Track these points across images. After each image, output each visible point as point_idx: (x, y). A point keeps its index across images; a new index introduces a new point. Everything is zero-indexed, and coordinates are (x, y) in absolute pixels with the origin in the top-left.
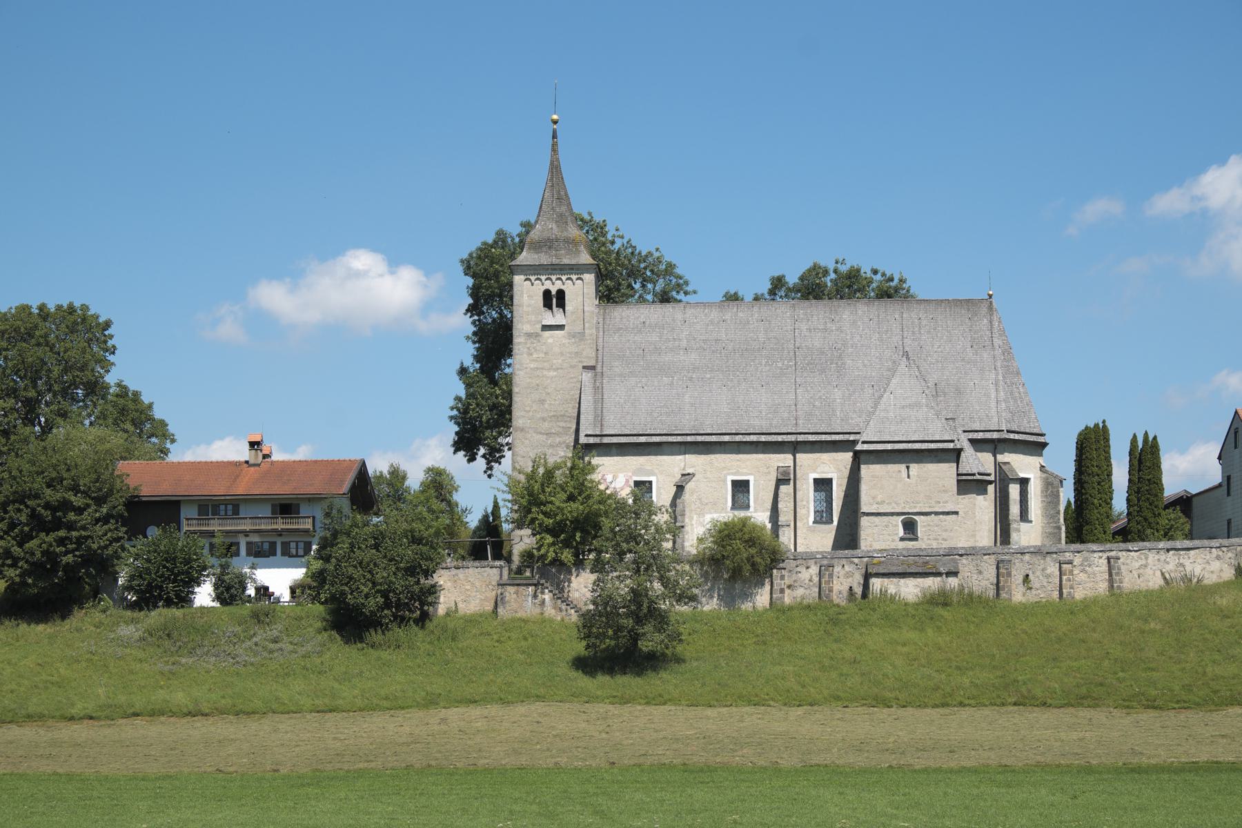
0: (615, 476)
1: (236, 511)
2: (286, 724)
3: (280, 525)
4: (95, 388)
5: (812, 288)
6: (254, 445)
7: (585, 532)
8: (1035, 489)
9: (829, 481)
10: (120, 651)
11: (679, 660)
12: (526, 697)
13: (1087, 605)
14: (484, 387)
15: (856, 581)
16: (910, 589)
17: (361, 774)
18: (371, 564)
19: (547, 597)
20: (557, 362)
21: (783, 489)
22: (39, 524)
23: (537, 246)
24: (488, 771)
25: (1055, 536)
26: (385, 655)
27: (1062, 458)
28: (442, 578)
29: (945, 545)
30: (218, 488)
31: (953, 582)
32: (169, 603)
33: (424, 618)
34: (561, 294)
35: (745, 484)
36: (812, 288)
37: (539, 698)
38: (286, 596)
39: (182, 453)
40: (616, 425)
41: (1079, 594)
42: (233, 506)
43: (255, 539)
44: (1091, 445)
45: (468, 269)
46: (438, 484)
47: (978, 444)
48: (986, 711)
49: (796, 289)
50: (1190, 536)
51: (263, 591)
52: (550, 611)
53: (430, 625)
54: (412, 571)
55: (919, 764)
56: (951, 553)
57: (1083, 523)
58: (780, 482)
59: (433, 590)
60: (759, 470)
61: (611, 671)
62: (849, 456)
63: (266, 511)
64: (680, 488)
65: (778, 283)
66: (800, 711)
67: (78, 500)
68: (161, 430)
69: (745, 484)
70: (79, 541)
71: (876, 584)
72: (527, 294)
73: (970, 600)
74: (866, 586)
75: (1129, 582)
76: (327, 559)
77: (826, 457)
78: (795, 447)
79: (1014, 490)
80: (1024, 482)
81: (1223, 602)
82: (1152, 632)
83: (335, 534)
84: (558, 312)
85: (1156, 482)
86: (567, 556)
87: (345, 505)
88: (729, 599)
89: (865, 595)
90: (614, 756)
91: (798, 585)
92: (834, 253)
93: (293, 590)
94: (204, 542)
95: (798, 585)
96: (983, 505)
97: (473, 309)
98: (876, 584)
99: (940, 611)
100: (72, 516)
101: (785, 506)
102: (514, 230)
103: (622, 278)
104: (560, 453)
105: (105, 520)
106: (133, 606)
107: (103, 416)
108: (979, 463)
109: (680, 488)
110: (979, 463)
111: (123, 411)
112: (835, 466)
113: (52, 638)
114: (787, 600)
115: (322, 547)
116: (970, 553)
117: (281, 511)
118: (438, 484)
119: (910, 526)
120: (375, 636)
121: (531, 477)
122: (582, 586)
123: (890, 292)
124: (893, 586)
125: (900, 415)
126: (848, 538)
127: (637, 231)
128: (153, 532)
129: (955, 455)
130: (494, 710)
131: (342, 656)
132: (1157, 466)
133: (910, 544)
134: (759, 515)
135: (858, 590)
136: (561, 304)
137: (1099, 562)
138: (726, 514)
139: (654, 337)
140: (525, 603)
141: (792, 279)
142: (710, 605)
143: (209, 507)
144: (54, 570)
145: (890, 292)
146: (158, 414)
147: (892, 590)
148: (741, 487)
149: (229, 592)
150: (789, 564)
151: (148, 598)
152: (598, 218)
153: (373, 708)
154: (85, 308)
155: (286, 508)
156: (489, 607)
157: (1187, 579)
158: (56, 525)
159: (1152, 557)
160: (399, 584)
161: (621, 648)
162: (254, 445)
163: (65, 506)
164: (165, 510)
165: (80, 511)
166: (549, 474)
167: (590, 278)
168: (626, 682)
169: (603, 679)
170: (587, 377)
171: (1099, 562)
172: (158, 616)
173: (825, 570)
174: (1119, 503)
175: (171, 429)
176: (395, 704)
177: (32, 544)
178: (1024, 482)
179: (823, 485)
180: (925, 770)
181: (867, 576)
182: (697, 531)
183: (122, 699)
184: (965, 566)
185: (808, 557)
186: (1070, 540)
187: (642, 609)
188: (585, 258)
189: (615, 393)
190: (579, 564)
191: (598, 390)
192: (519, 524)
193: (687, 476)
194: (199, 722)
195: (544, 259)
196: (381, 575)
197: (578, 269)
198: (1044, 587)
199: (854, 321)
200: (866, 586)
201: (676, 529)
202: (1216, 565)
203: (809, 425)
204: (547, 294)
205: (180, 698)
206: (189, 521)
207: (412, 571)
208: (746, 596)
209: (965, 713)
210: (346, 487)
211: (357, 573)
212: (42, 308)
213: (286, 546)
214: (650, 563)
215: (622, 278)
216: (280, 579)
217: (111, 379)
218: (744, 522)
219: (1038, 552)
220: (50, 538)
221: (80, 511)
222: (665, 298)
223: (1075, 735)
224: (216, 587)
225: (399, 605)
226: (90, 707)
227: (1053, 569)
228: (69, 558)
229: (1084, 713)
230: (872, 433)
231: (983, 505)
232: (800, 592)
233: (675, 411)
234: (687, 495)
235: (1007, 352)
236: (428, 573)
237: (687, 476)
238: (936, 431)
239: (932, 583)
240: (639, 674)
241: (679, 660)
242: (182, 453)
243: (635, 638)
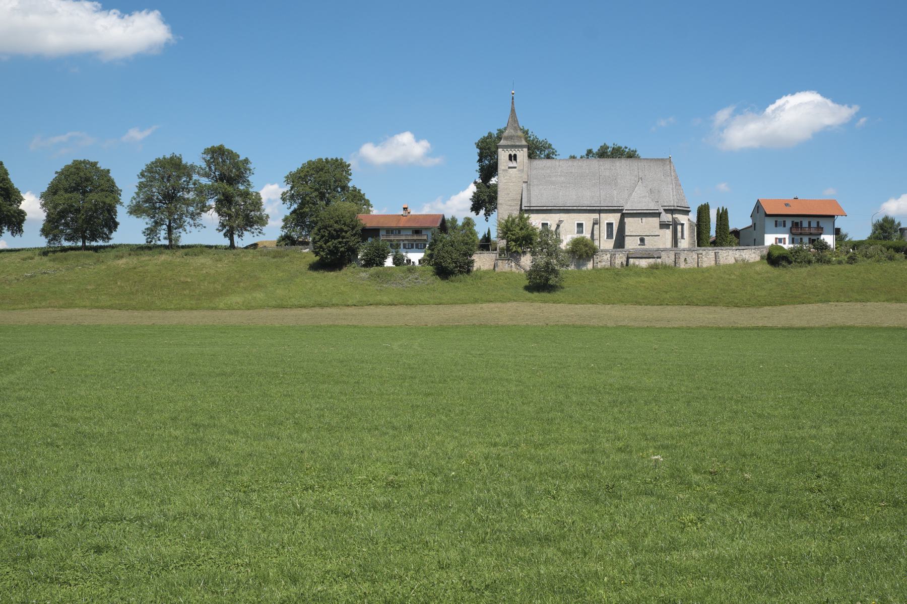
0: (536, 221)
1: (399, 232)
2: (425, 309)
3: (415, 237)
4: (344, 188)
5: (603, 154)
7: (526, 241)
8: (686, 227)
9: (612, 224)
10: (361, 282)
11: (563, 288)
12: (510, 300)
13: (708, 269)
14: (484, 189)
15: (624, 260)
16: (644, 263)
17: (457, 327)
18: (450, 253)
19: (513, 264)
20: (514, 180)
21: (596, 226)
22: (332, 237)
23: (507, 138)
24: (502, 326)
25: (694, 244)
26: (456, 284)
27: (693, 216)
28: (475, 257)
29: (655, 247)
30: (393, 224)
31: (659, 260)
32: (377, 265)
33: (469, 271)
34: (515, 156)
35: (582, 224)
36: (603, 154)
37: (515, 301)
38: (417, 263)
39: (374, 211)
40: (535, 203)
41: (705, 265)
42: (398, 231)
43: (406, 242)
44: (703, 211)
45: (478, 146)
46: (468, 223)
47: (666, 211)
48: (677, 307)
49: (597, 154)
50: (739, 244)
51: (409, 261)
52: (514, 269)
53: (472, 274)
54: (465, 255)
55: (658, 326)
56: (658, 250)
57: (701, 239)
58: (594, 224)
59: (472, 262)
60: (587, 220)
61: (538, 291)
62: (619, 215)
63: (410, 233)
64: (558, 226)
65: (589, 152)
66: (609, 306)
67: (346, 228)
68: (367, 203)
69: (582, 224)
70: (346, 243)
71: (631, 261)
72: (503, 155)
73: (665, 267)
74: (627, 261)
75: (722, 261)
76: (433, 250)
77: (611, 215)
78: (600, 211)
79: (679, 228)
80: (682, 225)
81: (758, 268)
82: (733, 279)
83: (435, 241)
84: (514, 162)
85: (727, 225)
86: (519, 250)
87: (437, 230)
88: (578, 266)
89: (627, 265)
90: (547, 322)
91: (603, 261)
93: (420, 261)
94: (388, 243)
95: (603, 261)
96: (668, 233)
97: (480, 161)
98: (631, 261)
99: (655, 271)
100: (344, 234)
101: (596, 232)
102: (495, 133)
103: (537, 150)
104: (516, 213)
105: (354, 235)
106: (364, 266)
107: (348, 198)
108: (667, 217)
109: (558, 226)
110: (667, 217)
111: (355, 196)
112: (614, 219)
113: (336, 277)
114: (599, 266)
115: (430, 246)
116: (665, 250)
117: (417, 232)
118: (468, 223)
119: (642, 240)
120: (453, 278)
121: (507, 221)
122: (526, 261)
123: (631, 155)
124: (637, 262)
125: (638, 200)
126: (620, 243)
127: (540, 134)
128: (370, 240)
129: (658, 215)
130: (499, 304)
131: (440, 284)
132: (727, 219)
133: (642, 247)
134: (587, 235)
135: (625, 263)
136: (515, 158)
137: (712, 254)
138: (576, 236)
139: (548, 171)
140: (505, 266)
141: (595, 150)
142: (572, 268)
143: (390, 231)
144: (337, 253)
145: (631, 155)
146: (366, 197)
147: (637, 263)
148: (580, 225)
149: (398, 261)
150: (600, 253)
151: (369, 263)
152: (526, 129)
153: (456, 303)
154: (341, 159)
155: (417, 231)
156: (492, 268)
157: (743, 260)
158: (338, 237)
159: (731, 252)
160: (461, 259)
161: (541, 283)
162: (543, 224)
163: (342, 230)
164: (374, 232)
165: (346, 232)
166: (513, 220)
167: (526, 150)
168: (545, 295)
169: (536, 294)
170: (524, 185)
171: (712, 254)
172: (374, 270)
173: (613, 256)
174: (713, 233)
175: (371, 203)
176: (463, 302)
177: (330, 244)
178: (682, 225)
179: (610, 225)
180: (661, 328)
181: (628, 258)
182: (565, 243)
183: (365, 299)
184: (663, 254)
185: (606, 251)
186: (699, 245)
187: (549, 269)
188: (524, 143)
189: (535, 191)
190: (524, 253)
191: (529, 190)
192: (136, 210)
193: (561, 221)
194: (394, 308)
195: (509, 143)
196: (454, 256)
197: (521, 147)
198: (692, 263)
199: (621, 166)
200: (627, 261)
201: (559, 241)
202: (753, 255)
204: (510, 155)
205: (385, 299)
206: (383, 237)
207: (465, 255)
208: (585, 265)
209: (669, 308)
210: (438, 225)
211: (446, 255)
212: (326, 159)
213: (417, 245)
214: (553, 251)
215: (537, 150)
216: (415, 257)
217: (350, 185)
218: (583, 238)
219: (689, 250)
220: (336, 241)
221: (346, 232)
222: (548, 157)
223: (711, 316)
224: (394, 259)
225: (460, 267)
226: (355, 302)
227: (695, 256)
228: (342, 249)
229: (712, 308)
230: (628, 207)
231: (668, 233)
232: (603, 263)
233: (556, 196)
234: (561, 228)
235: (676, 177)
236: (470, 256)
237: (561, 221)
238: (652, 206)
239: (652, 261)
240: (549, 292)
241: (563, 288)
242: (374, 211)
243: (547, 279)
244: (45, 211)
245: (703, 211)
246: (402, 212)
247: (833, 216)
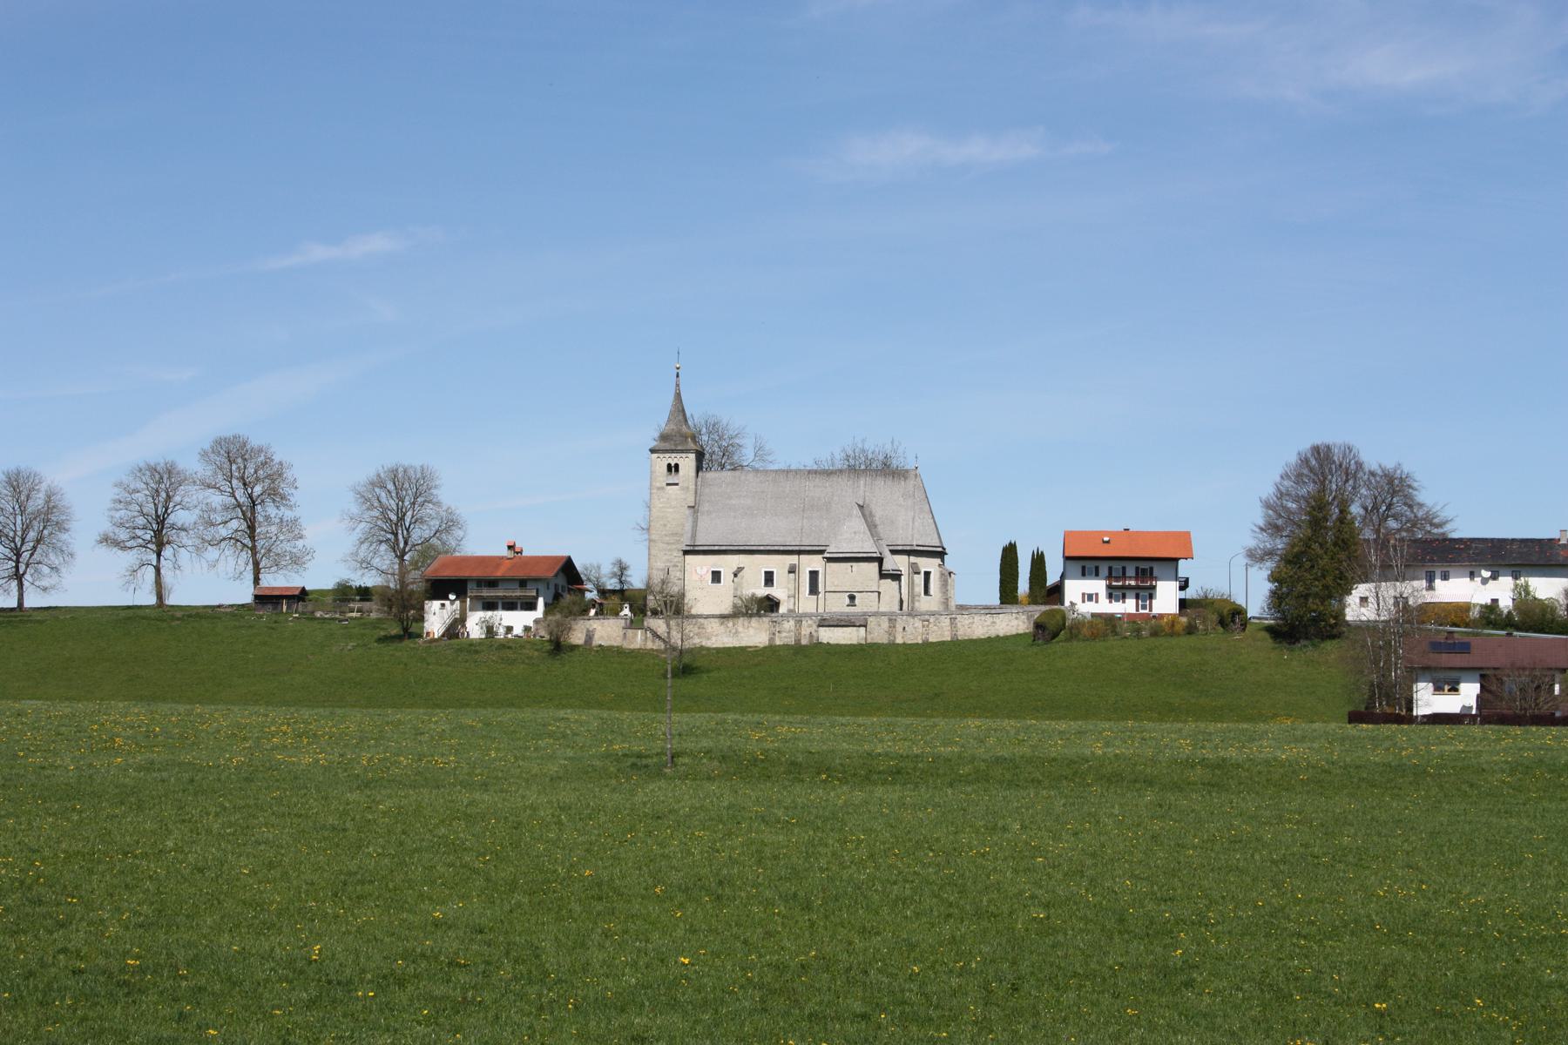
6: (510, 547)
28: (320, 576)
34: (677, 466)
56: (865, 614)
60: (778, 564)
78: (799, 553)
80: (927, 574)
92: (876, 443)
112: (815, 562)
119: (852, 598)
133: (852, 609)
162: (510, 547)
184: (872, 621)
189: (703, 522)
202: (1015, 622)
203: (807, 541)
204: (669, 466)
230: (834, 549)
237: (740, 569)
238: (868, 546)
244: (1374, 467)
245: (1010, 554)
246: (505, 552)
247: (1176, 560)
